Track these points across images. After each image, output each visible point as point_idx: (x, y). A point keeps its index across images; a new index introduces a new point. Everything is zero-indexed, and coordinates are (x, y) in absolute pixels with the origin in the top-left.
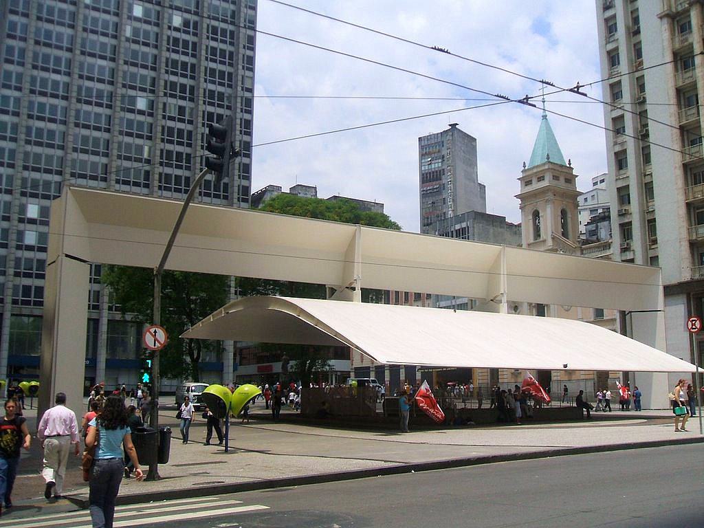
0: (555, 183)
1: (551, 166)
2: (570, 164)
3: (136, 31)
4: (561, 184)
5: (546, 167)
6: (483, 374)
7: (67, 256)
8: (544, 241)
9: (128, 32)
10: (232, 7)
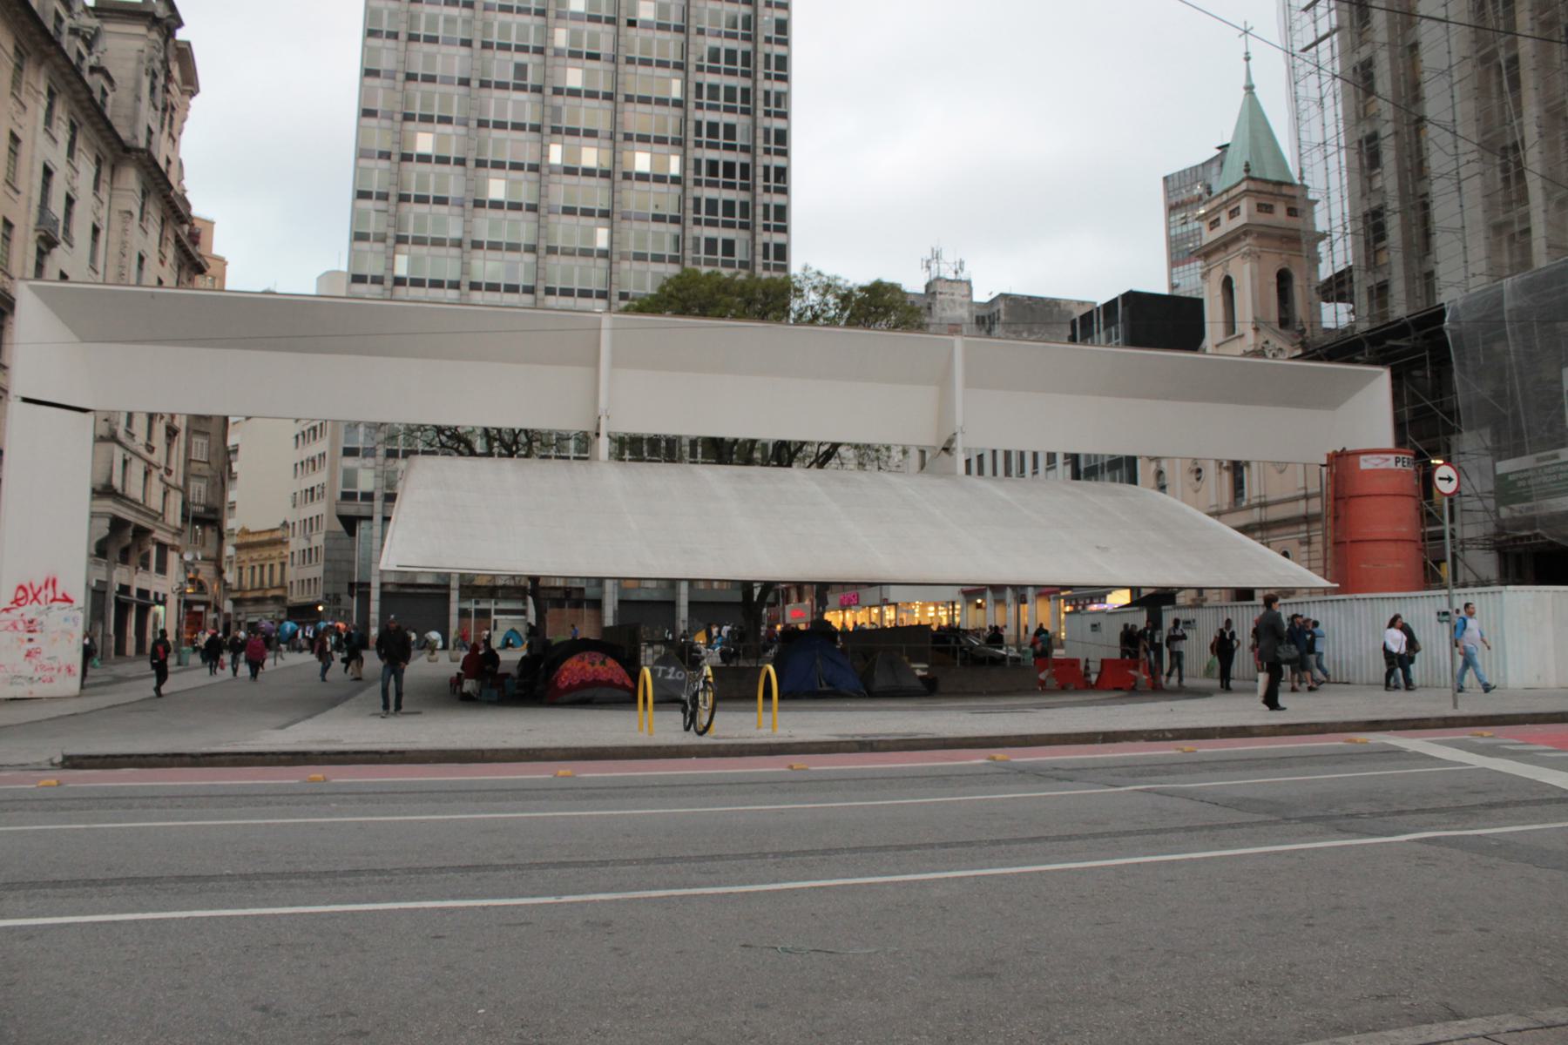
0: (1263, 218)
1: (1252, 186)
2: (1302, 178)
3: (574, 36)
4: (1280, 215)
5: (1244, 186)
6: (446, 265)
7: (26, 400)
8: (1241, 336)
9: (561, 38)
10: (744, 10)
